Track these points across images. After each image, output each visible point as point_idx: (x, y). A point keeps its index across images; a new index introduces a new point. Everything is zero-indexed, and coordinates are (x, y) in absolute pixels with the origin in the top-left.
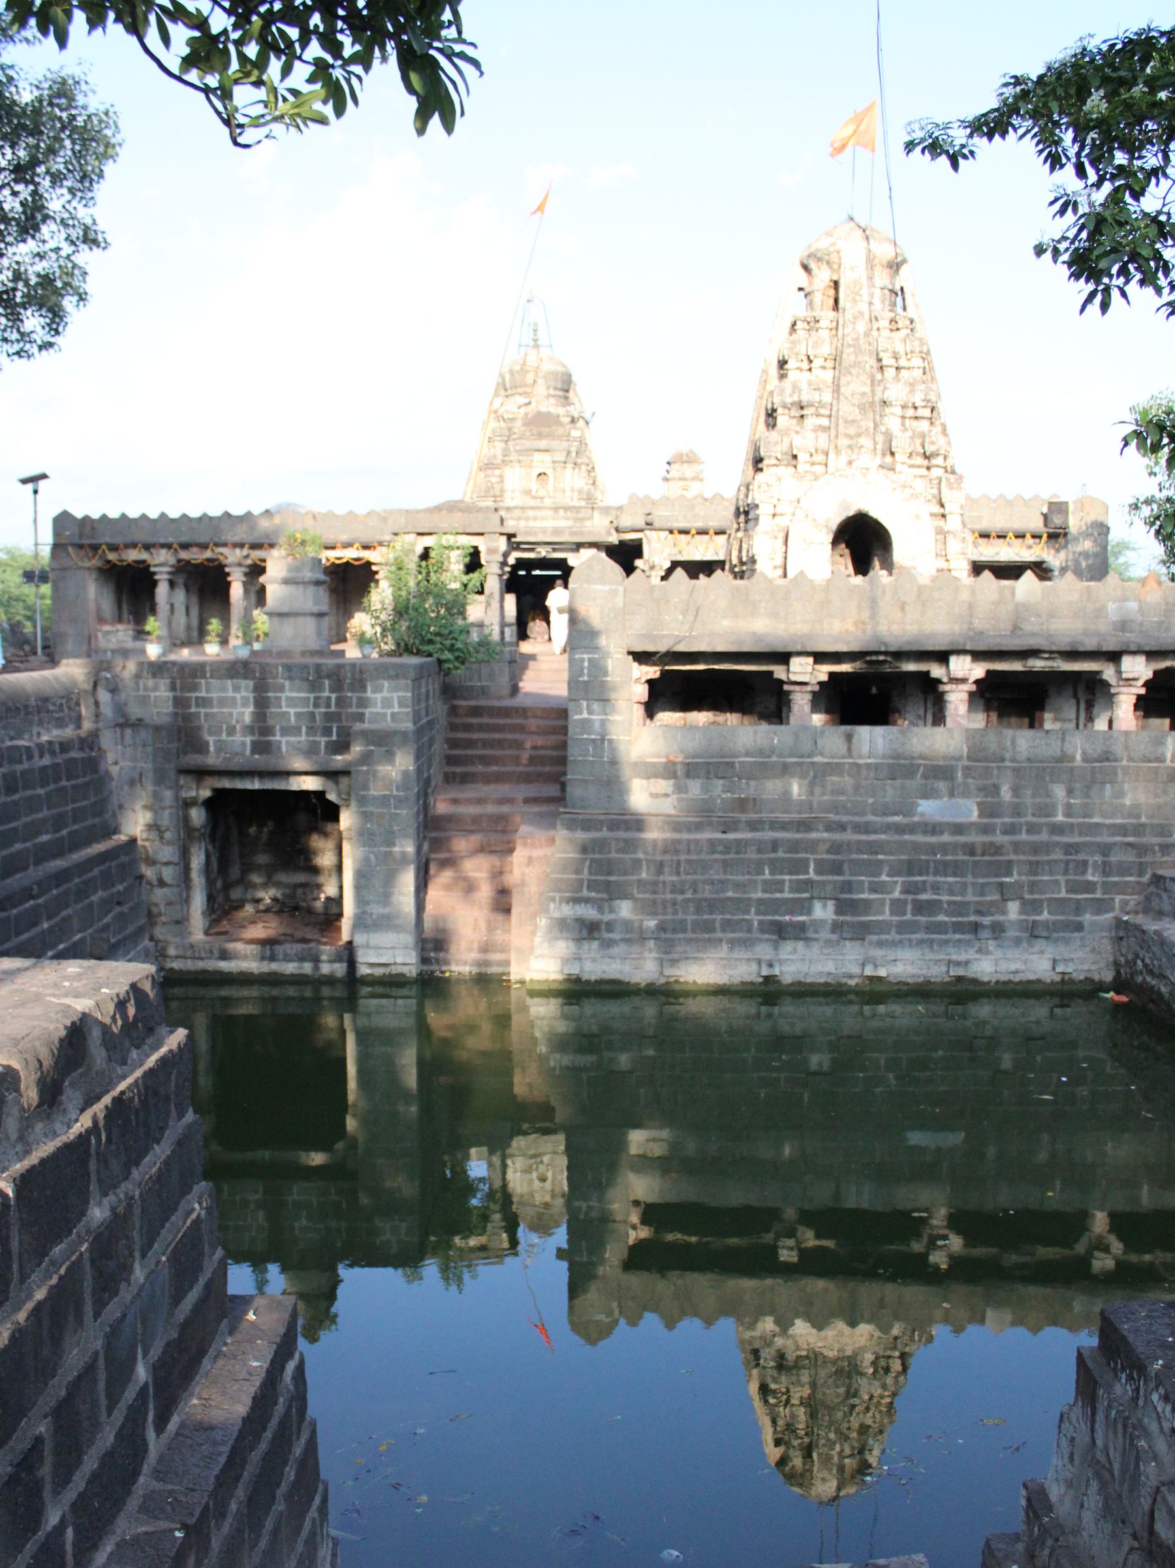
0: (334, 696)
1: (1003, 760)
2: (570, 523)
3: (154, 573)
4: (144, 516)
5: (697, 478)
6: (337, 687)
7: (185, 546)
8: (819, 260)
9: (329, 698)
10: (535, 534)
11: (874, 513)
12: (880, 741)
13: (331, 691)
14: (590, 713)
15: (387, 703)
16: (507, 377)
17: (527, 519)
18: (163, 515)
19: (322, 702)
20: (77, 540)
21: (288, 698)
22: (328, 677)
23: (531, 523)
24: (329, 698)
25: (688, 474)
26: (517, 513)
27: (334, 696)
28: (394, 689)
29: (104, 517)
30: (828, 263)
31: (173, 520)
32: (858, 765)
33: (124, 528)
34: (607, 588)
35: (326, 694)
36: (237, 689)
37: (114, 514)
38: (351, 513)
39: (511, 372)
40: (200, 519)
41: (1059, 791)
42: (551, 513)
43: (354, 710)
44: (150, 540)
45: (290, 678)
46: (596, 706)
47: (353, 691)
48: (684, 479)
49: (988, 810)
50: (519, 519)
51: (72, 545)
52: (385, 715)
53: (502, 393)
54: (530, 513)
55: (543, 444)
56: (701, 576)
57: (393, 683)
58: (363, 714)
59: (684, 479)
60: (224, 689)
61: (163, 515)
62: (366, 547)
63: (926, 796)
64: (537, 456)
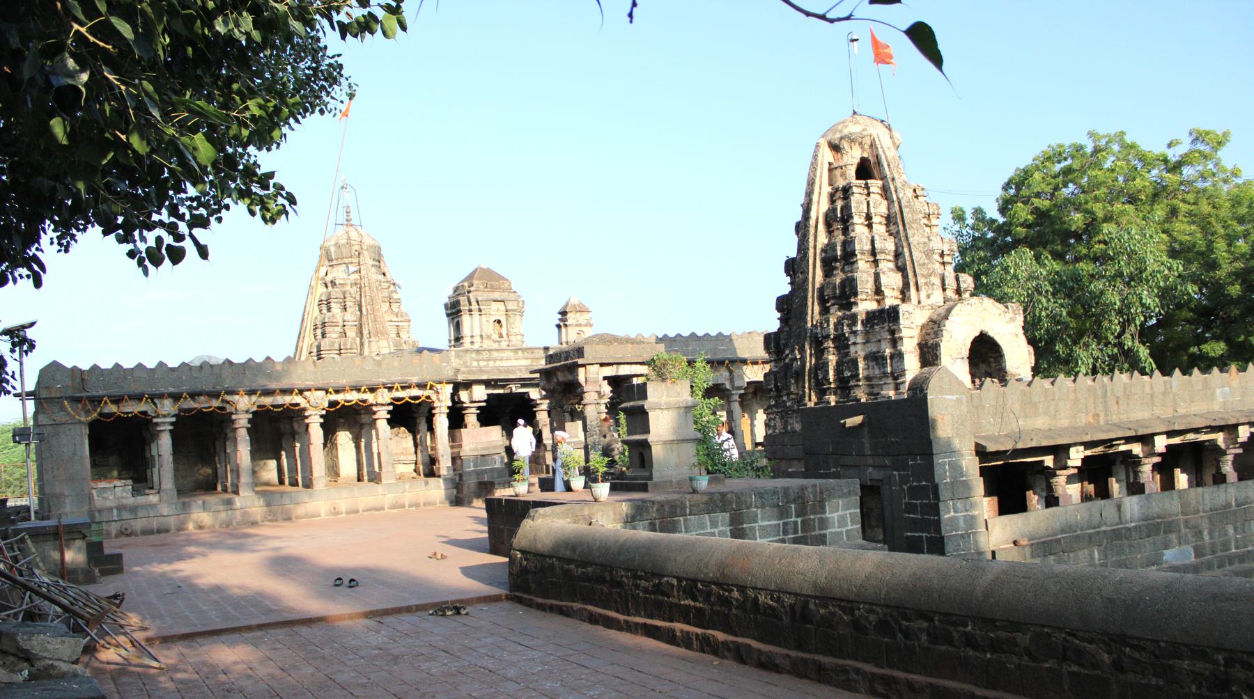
0: (799, 520)
1: (1198, 511)
2: (528, 362)
3: (157, 424)
4: (140, 366)
5: (589, 325)
6: (801, 512)
7: (193, 395)
8: (852, 141)
9: (796, 523)
10: (513, 372)
11: (991, 334)
12: (1136, 507)
13: (797, 516)
14: (955, 512)
15: (842, 521)
16: (333, 249)
17: (495, 360)
18: (161, 364)
19: (790, 527)
20: (70, 393)
21: (762, 528)
22: (794, 501)
23: (498, 363)
24: (796, 523)
25: (582, 321)
26: (485, 355)
27: (799, 520)
28: (847, 507)
29: (95, 368)
30: (860, 144)
31: (172, 369)
32: (1129, 529)
33: (119, 383)
34: (954, 397)
35: (793, 519)
36: (714, 524)
37: (106, 364)
38: (720, 334)
39: (337, 245)
40: (201, 367)
41: (1231, 530)
42: (512, 354)
43: (817, 532)
44: (149, 390)
45: (763, 506)
46: (959, 504)
47: (813, 513)
48: (580, 325)
49: (1199, 552)
50: (488, 360)
51: (67, 398)
52: (841, 533)
53: (327, 263)
54: (495, 354)
55: (496, 295)
56: (1196, 371)
57: (846, 500)
58: (824, 536)
59: (580, 325)
60: (702, 526)
61: (161, 364)
62: (337, 392)
63: (1167, 547)
64: (495, 306)
